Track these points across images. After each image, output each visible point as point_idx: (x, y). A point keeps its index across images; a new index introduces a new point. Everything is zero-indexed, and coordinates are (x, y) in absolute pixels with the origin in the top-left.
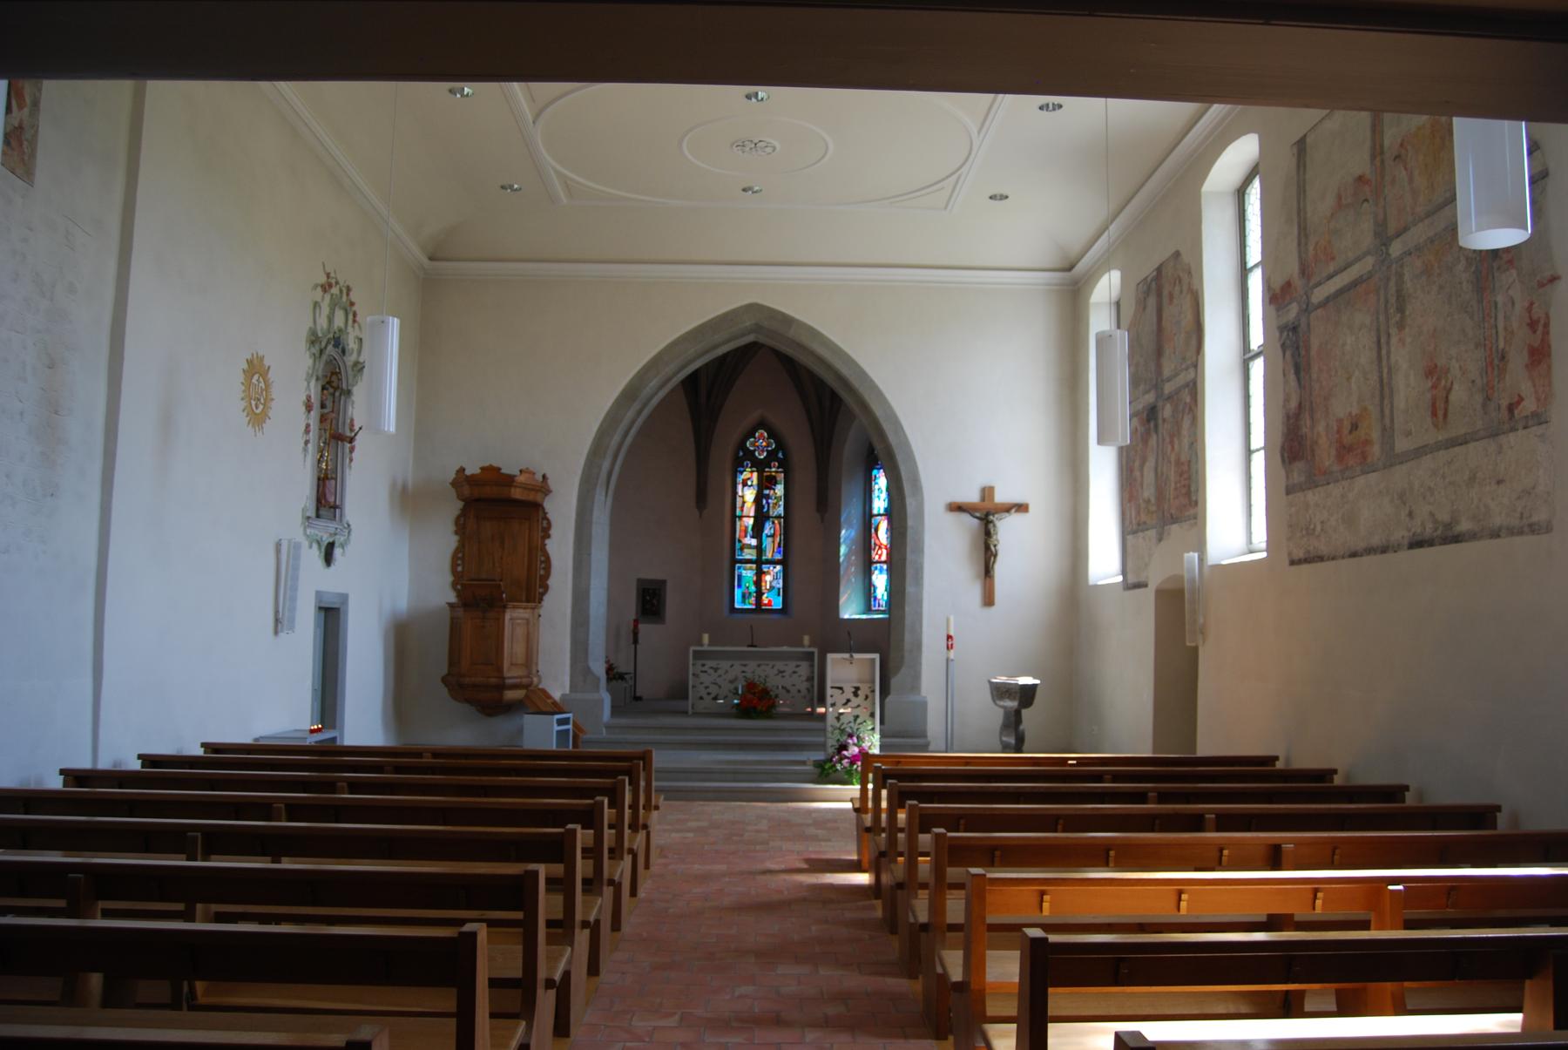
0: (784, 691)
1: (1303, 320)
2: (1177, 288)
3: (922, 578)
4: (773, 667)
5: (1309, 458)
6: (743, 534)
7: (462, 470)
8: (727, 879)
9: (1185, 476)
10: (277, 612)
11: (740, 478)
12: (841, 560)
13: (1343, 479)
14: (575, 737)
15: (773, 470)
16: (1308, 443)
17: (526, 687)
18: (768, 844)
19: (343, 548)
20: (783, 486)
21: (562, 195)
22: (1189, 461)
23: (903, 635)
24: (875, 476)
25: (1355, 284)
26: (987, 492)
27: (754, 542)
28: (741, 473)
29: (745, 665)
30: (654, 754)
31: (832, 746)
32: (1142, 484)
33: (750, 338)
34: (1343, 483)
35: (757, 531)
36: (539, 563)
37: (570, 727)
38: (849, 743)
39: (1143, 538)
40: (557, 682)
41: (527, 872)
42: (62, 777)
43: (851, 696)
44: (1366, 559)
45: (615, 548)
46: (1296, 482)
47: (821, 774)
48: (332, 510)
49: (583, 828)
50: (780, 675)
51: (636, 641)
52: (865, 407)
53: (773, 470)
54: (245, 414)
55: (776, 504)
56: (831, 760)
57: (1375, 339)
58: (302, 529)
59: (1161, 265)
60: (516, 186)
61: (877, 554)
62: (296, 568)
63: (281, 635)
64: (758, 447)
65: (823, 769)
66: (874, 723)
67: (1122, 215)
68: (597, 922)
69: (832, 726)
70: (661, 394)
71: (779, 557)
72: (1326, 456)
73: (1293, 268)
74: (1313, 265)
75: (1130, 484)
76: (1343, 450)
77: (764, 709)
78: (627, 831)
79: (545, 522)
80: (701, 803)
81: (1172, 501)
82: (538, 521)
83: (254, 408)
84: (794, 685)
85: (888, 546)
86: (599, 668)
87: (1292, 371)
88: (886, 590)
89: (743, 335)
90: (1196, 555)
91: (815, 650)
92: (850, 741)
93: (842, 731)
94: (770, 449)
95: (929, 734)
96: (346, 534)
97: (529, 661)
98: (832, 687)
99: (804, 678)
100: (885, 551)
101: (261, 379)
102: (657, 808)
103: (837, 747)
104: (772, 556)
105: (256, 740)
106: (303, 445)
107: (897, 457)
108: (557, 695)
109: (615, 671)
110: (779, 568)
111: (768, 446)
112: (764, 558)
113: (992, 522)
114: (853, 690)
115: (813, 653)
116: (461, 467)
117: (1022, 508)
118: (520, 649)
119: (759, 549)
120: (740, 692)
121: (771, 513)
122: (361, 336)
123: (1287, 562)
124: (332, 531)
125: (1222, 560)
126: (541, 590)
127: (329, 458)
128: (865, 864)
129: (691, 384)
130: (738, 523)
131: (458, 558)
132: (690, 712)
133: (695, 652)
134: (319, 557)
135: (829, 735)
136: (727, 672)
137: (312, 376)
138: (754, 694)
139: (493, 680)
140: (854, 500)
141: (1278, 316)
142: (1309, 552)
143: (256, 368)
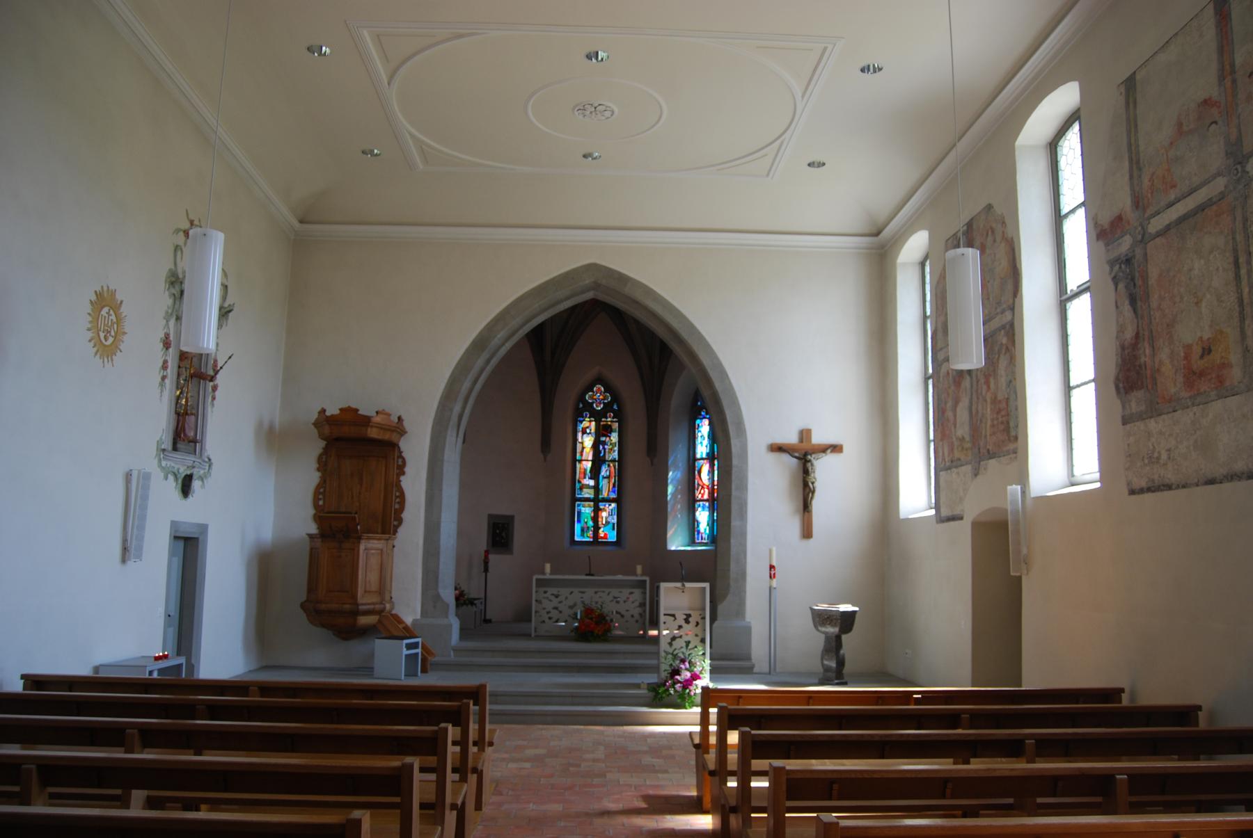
0: (619, 616)
1: (1139, 252)
2: (990, 238)
3: (746, 512)
5: (1150, 387)
6: (582, 476)
7: (323, 411)
8: (562, 824)
9: (1003, 413)
10: (125, 541)
12: (669, 498)
13: (1193, 405)
14: (424, 660)
15: (609, 419)
16: (1148, 372)
17: (380, 612)
18: (605, 776)
19: (202, 480)
20: (617, 434)
21: (418, 160)
22: (1008, 399)
23: (729, 565)
24: (698, 425)
25: (1201, 208)
26: (805, 434)
27: (592, 483)
28: (581, 422)
29: (583, 592)
31: (665, 670)
32: (955, 425)
34: (1195, 409)
35: (595, 473)
37: (419, 650)
38: (681, 668)
39: (958, 473)
40: (409, 609)
41: (404, 765)
42: (23, 681)
43: (683, 623)
44: (1227, 486)
45: (465, 486)
46: (1134, 411)
47: (656, 696)
48: (192, 444)
49: (453, 726)
50: (615, 600)
51: (486, 570)
53: (609, 419)
54: (92, 344)
55: (611, 449)
56: (664, 685)
57: (1231, 259)
58: (156, 461)
59: (972, 219)
60: (376, 151)
62: (145, 498)
63: (130, 563)
64: (595, 399)
65: (657, 693)
66: (704, 649)
67: (933, 175)
68: (463, 803)
69: (665, 652)
70: (509, 345)
71: (613, 496)
72: (1171, 382)
73: (1124, 201)
74: (1149, 195)
75: (942, 425)
76: (1192, 377)
77: (600, 633)
78: (451, 777)
79: (400, 460)
80: (541, 726)
81: (988, 437)
82: (394, 459)
83: (104, 341)
84: (627, 611)
85: (710, 486)
86: (448, 595)
87: (1127, 302)
88: (708, 525)
89: (583, 292)
90: (1019, 487)
91: (647, 579)
92: (682, 666)
93: (675, 657)
94: (606, 401)
95: (753, 658)
96: (207, 468)
97: (383, 589)
98: (665, 615)
99: (637, 604)
100: (707, 491)
101: (112, 312)
102: (491, 744)
103: (670, 671)
104: (608, 495)
105: (96, 669)
106: (160, 380)
107: (723, 401)
108: (408, 620)
109: (466, 597)
110: (613, 505)
111: (604, 399)
112: (600, 496)
113: (810, 461)
114: (685, 617)
115: (645, 581)
116: (323, 408)
117: (836, 448)
118: (373, 577)
119: (597, 488)
120: (579, 617)
121: (607, 457)
122: (226, 284)
123: (1127, 492)
124: (190, 463)
125: (911, 514)
126: (396, 523)
127: (189, 395)
128: (707, 801)
129: (537, 336)
130: (578, 465)
131: (320, 492)
132: (533, 636)
133: (537, 580)
134: (176, 488)
135: (663, 660)
136: (566, 598)
137: (171, 314)
138: (591, 619)
139: (347, 607)
140: (680, 446)
141: (1108, 251)
142: (1153, 481)
143: (104, 301)
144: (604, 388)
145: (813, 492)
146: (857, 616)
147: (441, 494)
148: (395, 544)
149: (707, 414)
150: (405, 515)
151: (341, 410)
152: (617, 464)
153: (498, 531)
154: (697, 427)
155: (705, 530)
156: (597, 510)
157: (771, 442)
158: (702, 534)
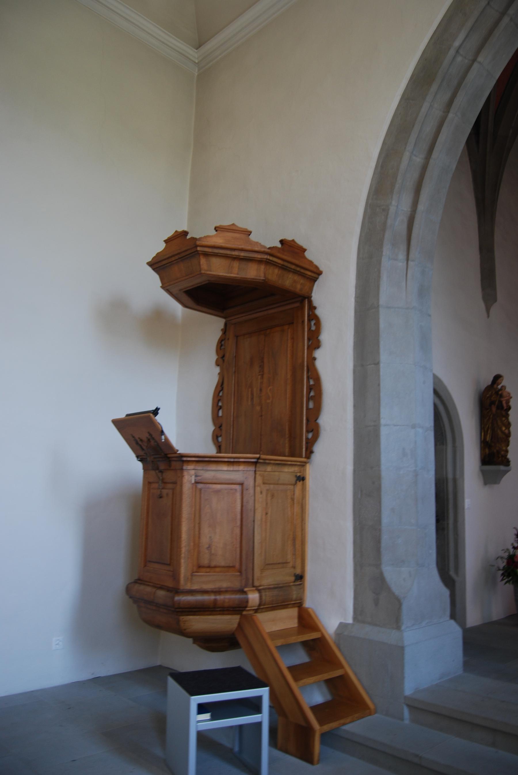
126: (310, 435)
147: (378, 370)
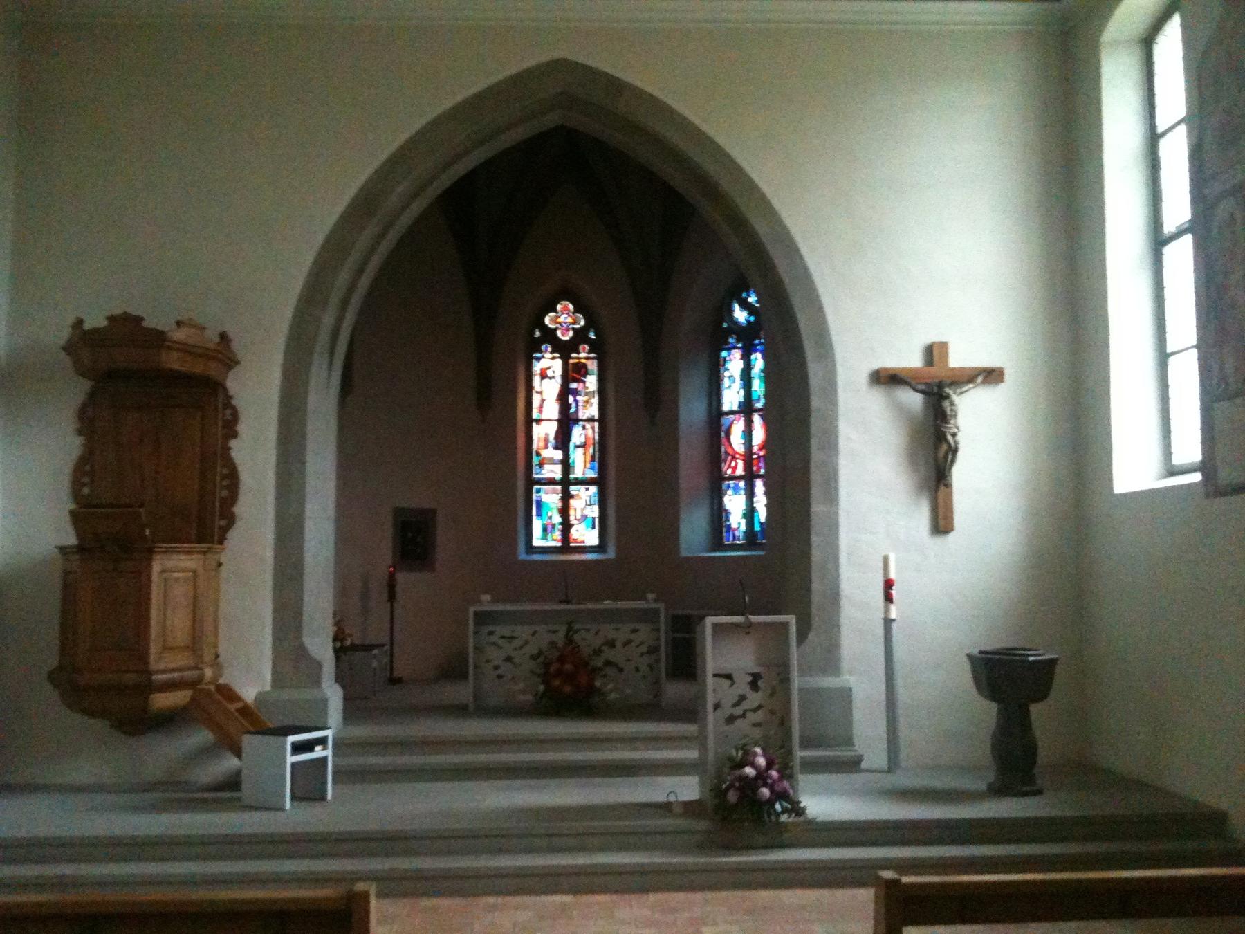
3: (836, 489)
4: (597, 633)
6: (542, 444)
7: (79, 322)
11: (537, 367)
15: (583, 355)
17: (193, 684)
26: (934, 353)
27: (558, 455)
30: (373, 902)
33: (551, 120)
35: (563, 440)
36: (218, 479)
43: (746, 690)
51: (392, 597)
52: (740, 224)
55: (587, 402)
61: (729, 467)
64: (560, 323)
70: (417, 208)
71: (591, 474)
79: (228, 412)
80: (491, 900)
86: (321, 646)
94: (577, 326)
95: (856, 740)
98: (715, 675)
99: (644, 649)
100: (740, 464)
104: (584, 474)
108: (249, 694)
111: (573, 324)
112: (572, 476)
114: (750, 679)
117: (992, 376)
118: (179, 622)
119: (566, 464)
126: (223, 523)
131: (84, 472)
133: (476, 614)
139: (130, 678)
144: (574, 305)
145: (955, 451)
146: (1059, 669)
148: (223, 560)
149: (738, 341)
150: (239, 509)
151: (112, 319)
152: (596, 424)
153: (410, 535)
154: (722, 363)
155: (739, 524)
156: (566, 497)
157: (877, 365)
158: (734, 530)
